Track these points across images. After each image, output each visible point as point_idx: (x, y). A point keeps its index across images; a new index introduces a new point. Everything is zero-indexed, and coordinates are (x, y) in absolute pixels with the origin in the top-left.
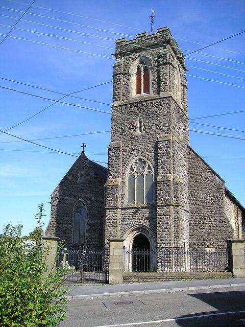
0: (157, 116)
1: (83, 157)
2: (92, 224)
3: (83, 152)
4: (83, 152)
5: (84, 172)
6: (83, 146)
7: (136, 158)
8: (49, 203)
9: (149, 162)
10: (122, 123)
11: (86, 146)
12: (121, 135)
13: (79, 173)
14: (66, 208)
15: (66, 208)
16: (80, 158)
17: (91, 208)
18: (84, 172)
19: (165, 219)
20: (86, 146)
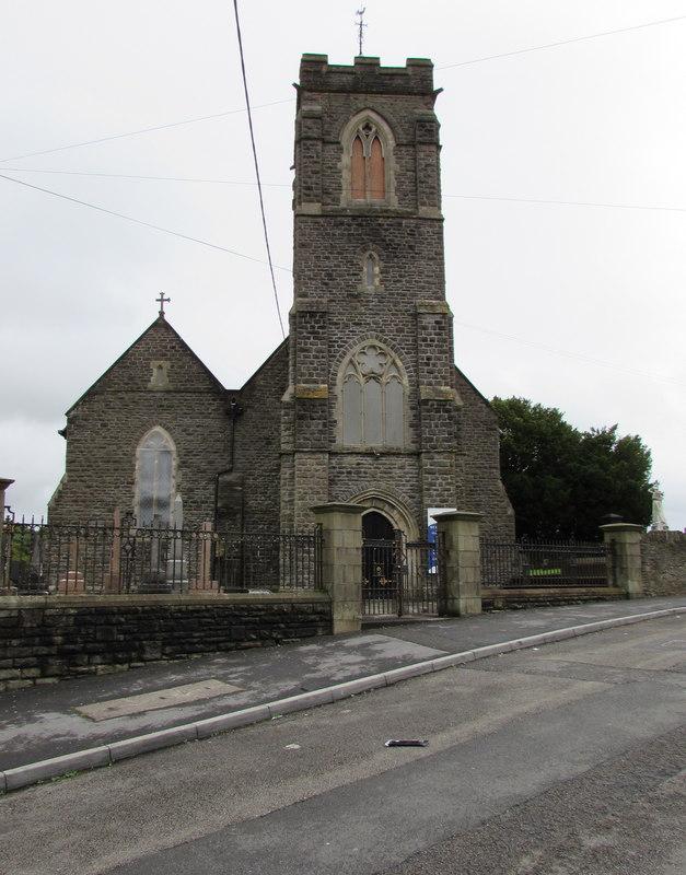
0: (413, 257)
1: (161, 325)
2: (191, 490)
3: (162, 313)
4: (162, 313)
5: (166, 364)
6: (162, 300)
7: (365, 343)
8: (615, 428)
9: (393, 354)
10: (327, 258)
11: (162, 294)
12: (326, 284)
13: (154, 364)
14: (115, 447)
15: (115, 447)
16: (155, 325)
17: (188, 452)
18: (166, 364)
19: (440, 481)
20: (168, 300)
